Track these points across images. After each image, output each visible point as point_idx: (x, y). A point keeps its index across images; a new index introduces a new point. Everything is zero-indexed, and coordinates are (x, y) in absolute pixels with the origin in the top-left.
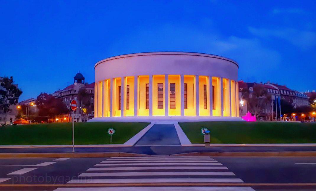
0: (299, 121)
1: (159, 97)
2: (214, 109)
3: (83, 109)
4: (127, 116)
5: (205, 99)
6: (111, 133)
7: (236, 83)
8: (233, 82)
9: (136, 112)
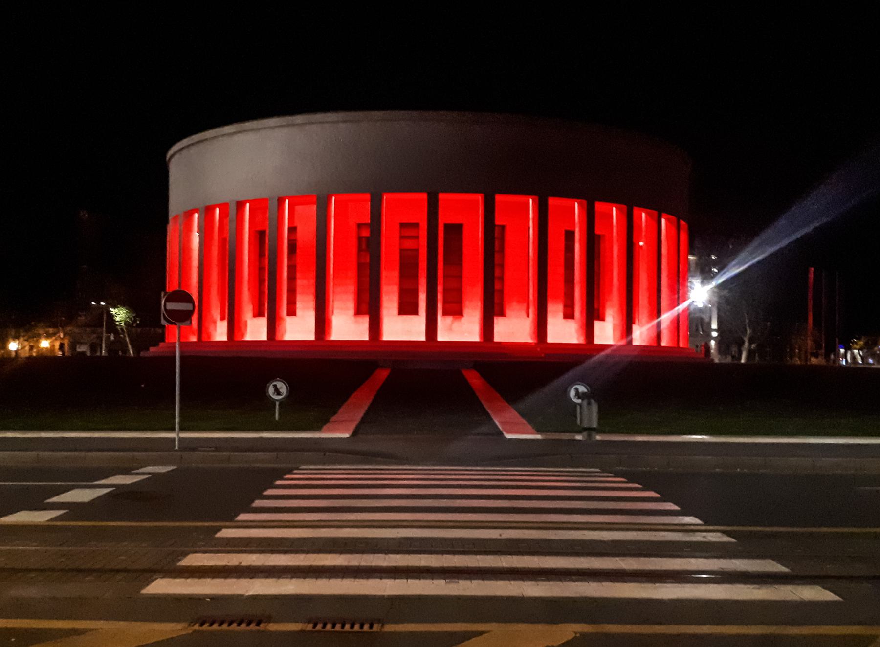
2: (745, 244)
3: (114, 311)
6: (279, 393)
9: (322, 323)
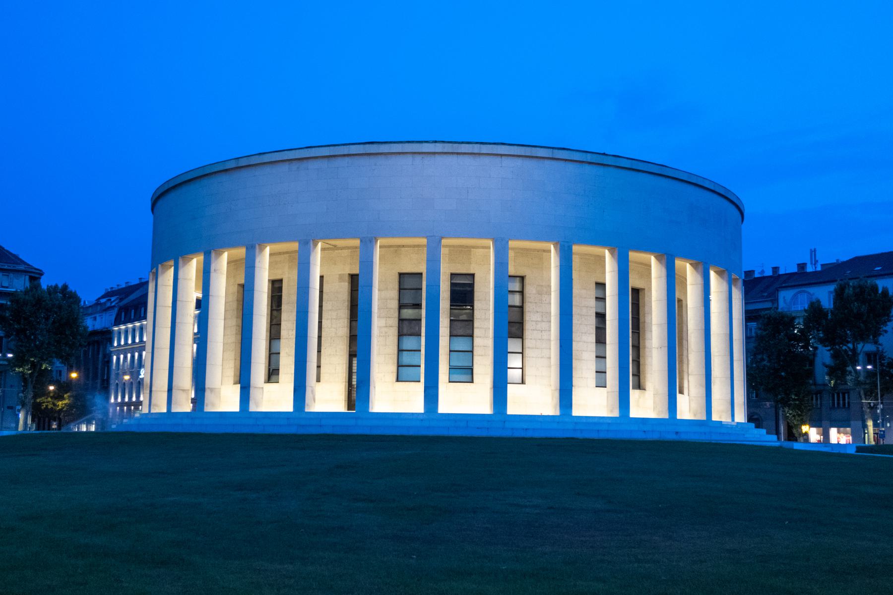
0: (354, 237)
1: (455, 333)
4: (265, 407)
5: (601, 339)
7: (731, 283)
8: (719, 273)
